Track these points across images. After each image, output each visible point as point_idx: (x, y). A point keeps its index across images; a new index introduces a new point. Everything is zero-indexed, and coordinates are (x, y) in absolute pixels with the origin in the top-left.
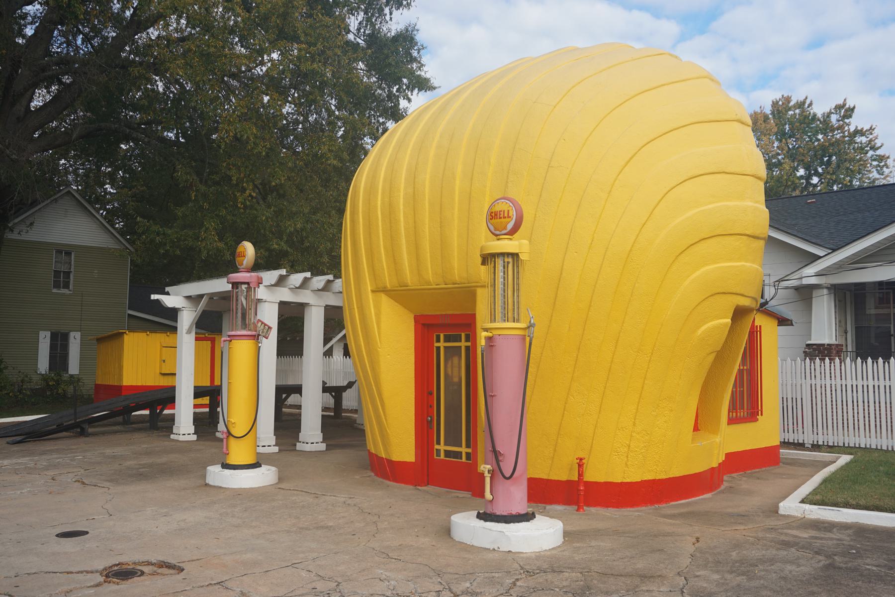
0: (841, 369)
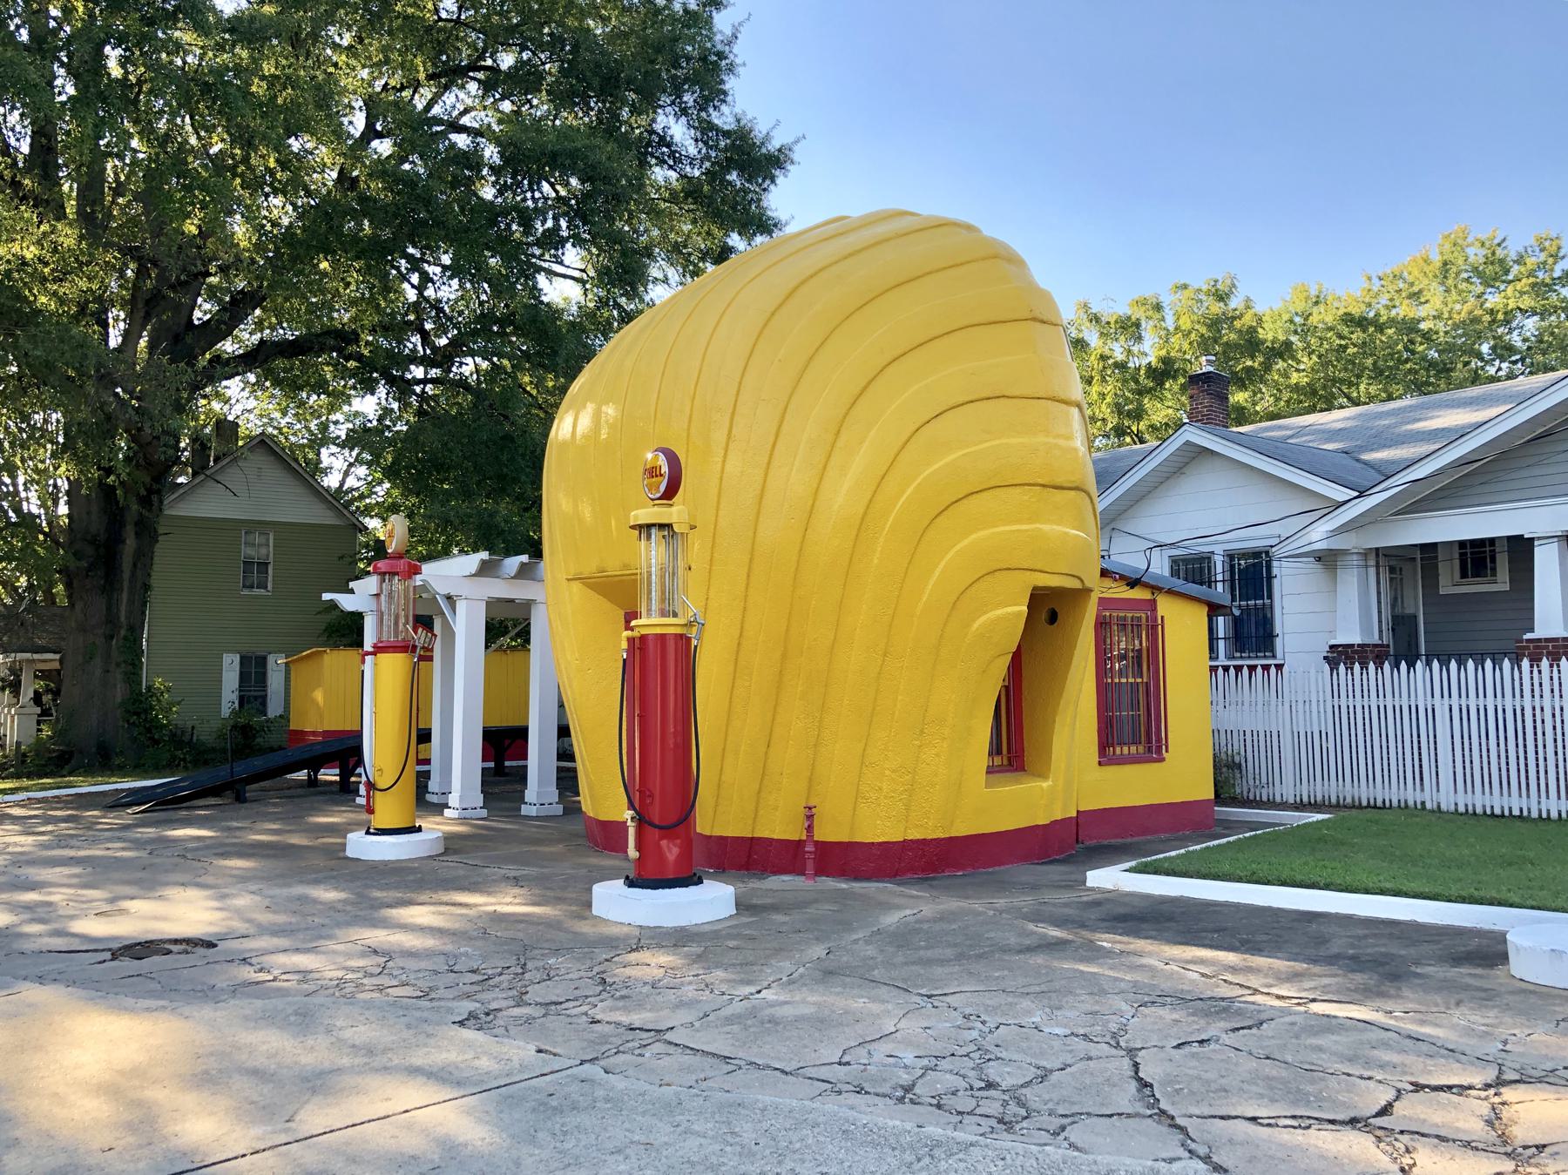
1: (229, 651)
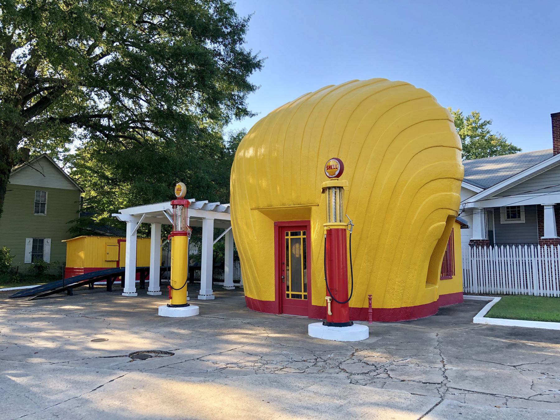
0: (487, 252)
1: (28, 237)
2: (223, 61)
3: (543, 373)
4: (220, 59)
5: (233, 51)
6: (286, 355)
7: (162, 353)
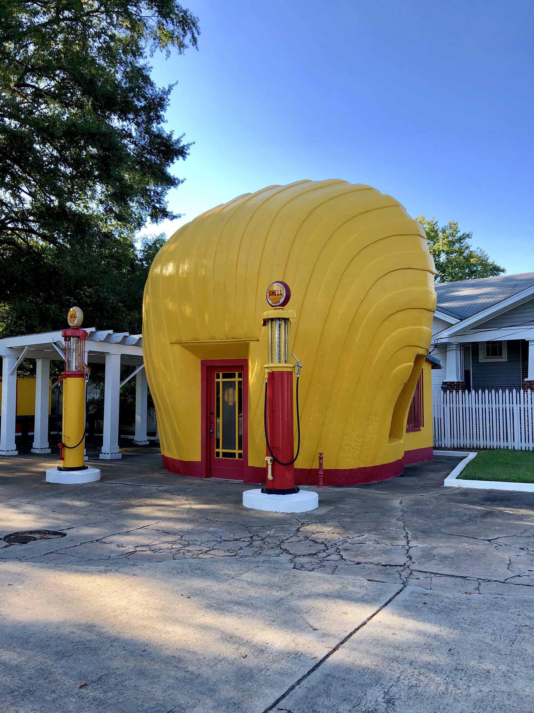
2: (135, 144)
3: (522, 549)
4: (131, 143)
5: (148, 132)
6: (214, 533)
7: (49, 534)
